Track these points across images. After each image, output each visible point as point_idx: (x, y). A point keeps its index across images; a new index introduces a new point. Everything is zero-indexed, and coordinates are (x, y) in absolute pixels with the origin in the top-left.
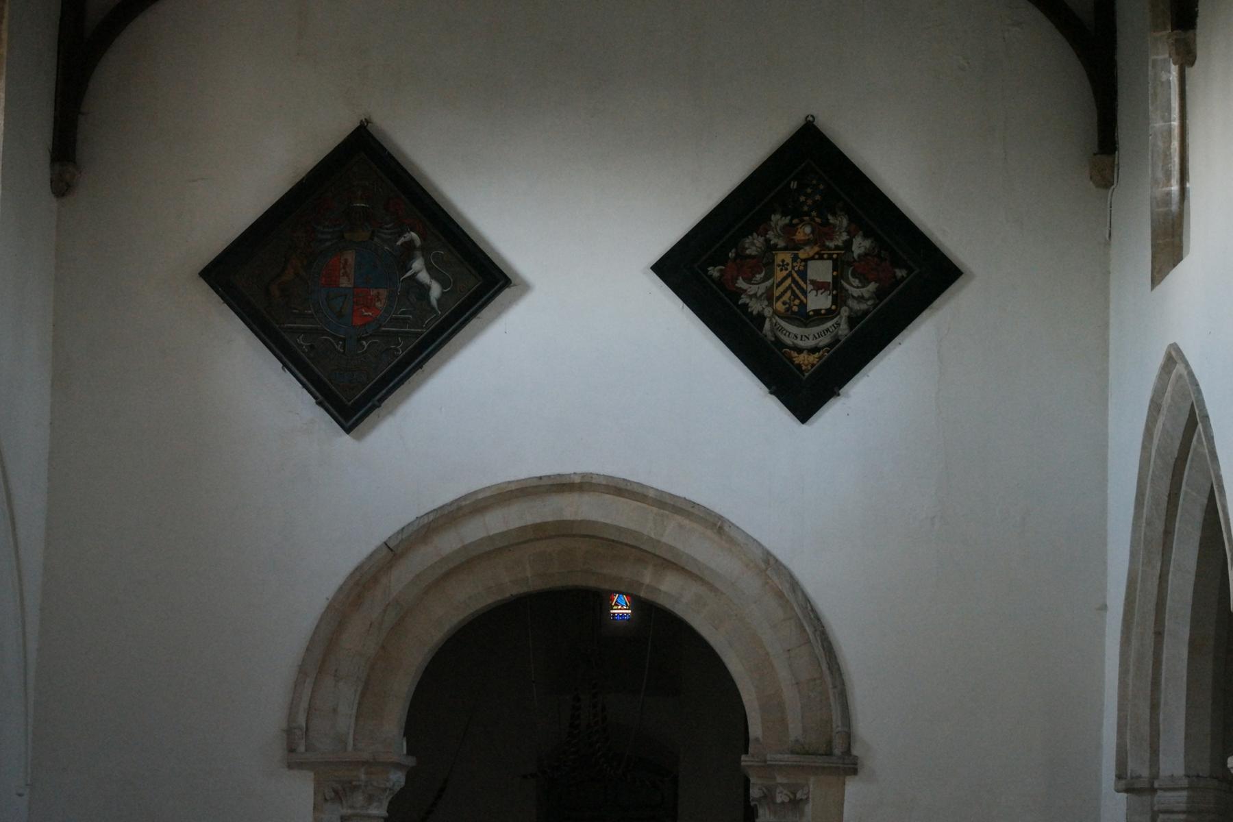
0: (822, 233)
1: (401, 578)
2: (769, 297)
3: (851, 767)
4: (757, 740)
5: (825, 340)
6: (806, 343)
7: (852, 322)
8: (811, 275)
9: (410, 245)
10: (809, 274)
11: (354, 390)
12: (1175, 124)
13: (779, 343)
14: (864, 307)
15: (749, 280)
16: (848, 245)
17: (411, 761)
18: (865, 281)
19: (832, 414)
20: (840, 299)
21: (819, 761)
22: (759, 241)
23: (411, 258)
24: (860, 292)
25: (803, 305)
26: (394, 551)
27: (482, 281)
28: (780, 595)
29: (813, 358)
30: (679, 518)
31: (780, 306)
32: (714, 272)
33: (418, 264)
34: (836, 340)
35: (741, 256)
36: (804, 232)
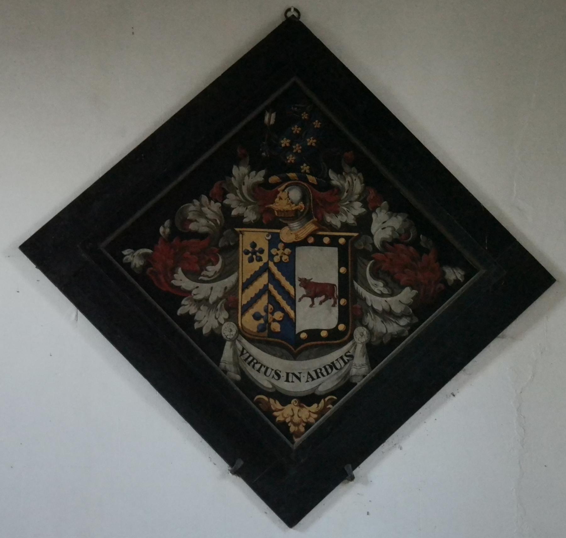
5: (328, 383)
6: (299, 388)
7: (375, 351)
13: (249, 386)
14: (393, 328)
15: (194, 275)
16: (364, 223)
20: (352, 313)
22: (212, 209)
24: (387, 304)
25: (289, 322)
29: (307, 413)
31: (249, 322)
32: (134, 258)
34: (347, 384)
35: (181, 233)
36: (290, 197)
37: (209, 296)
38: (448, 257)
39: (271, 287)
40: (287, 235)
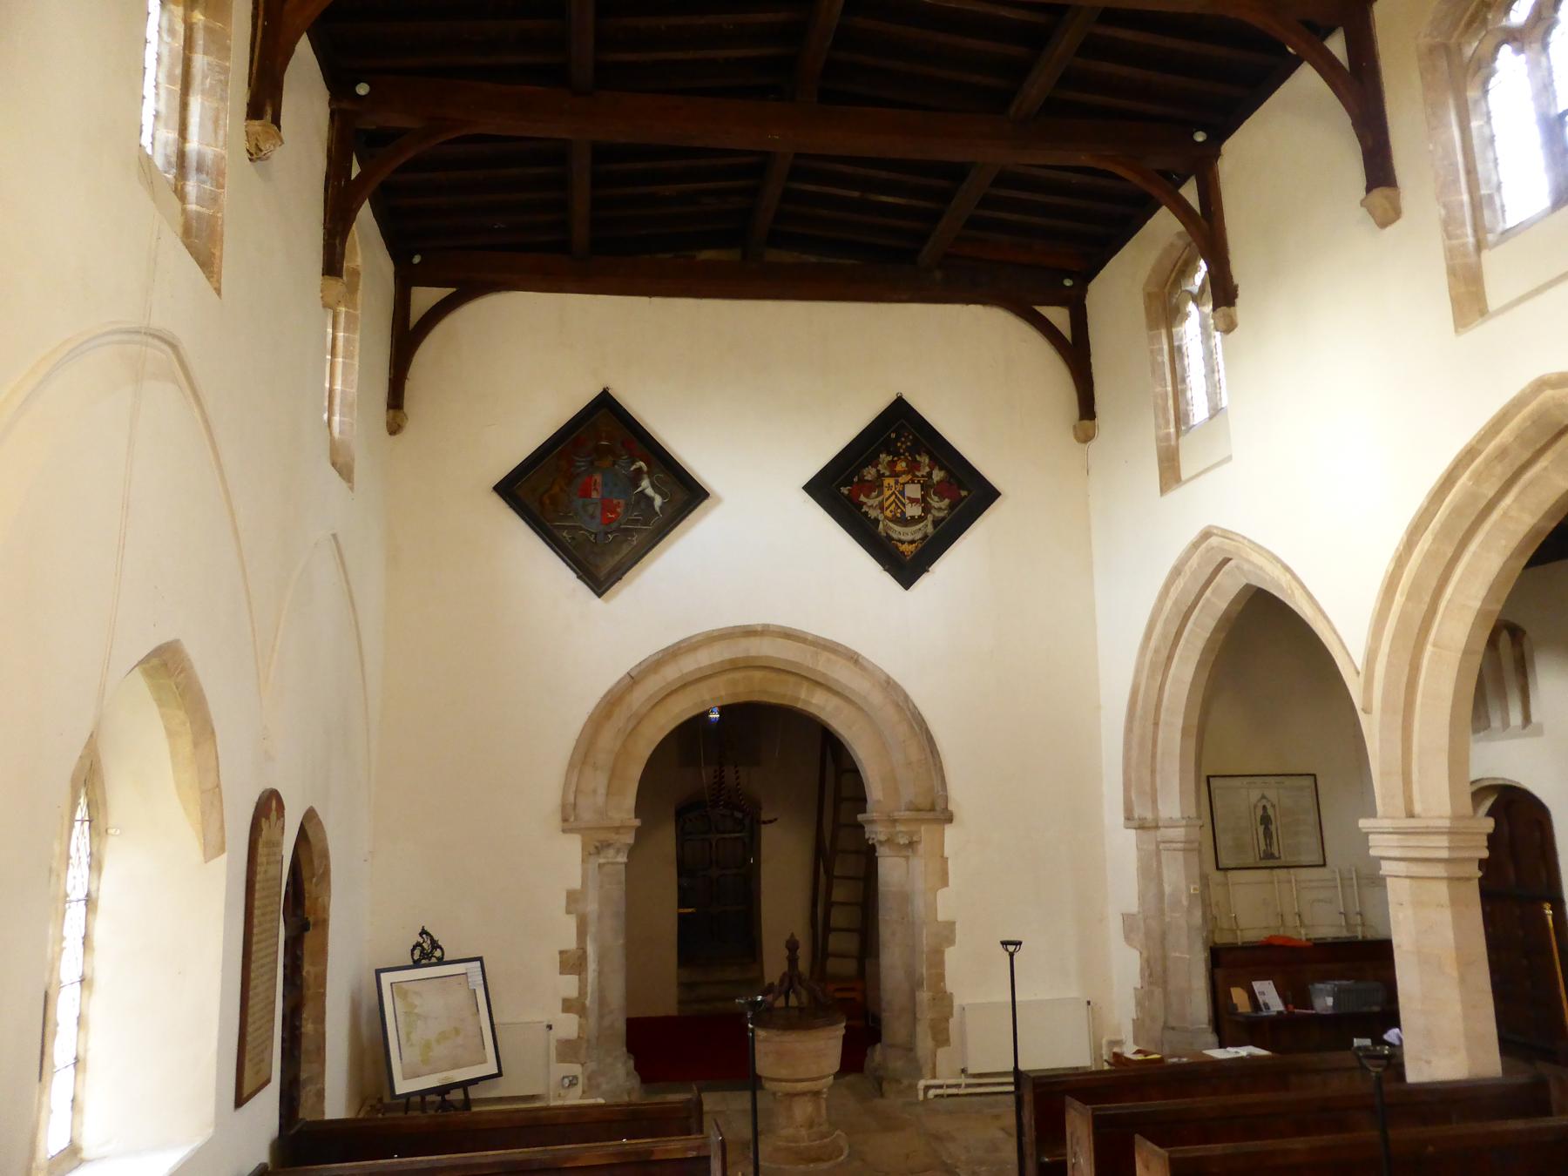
0: (913, 466)
1: (639, 698)
2: (881, 507)
3: (950, 819)
4: (879, 802)
5: (918, 536)
6: (907, 537)
7: (936, 523)
8: (907, 494)
9: (640, 469)
10: (906, 491)
11: (599, 568)
12: (1169, 389)
13: (889, 538)
14: (942, 514)
15: (867, 496)
16: (930, 475)
17: (637, 823)
18: (942, 498)
19: (924, 583)
20: (927, 509)
21: (930, 815)
22: (873, 471)
23: (641, 479)
24: (940, 505)
25: (903, 513)
26: (633, 680)
27: (688, 494)
28: (898, 705)
29: (912, 547)
30: (826, 654)
31: (888, 513)
32: (845, 490)
33: (645, 483)
34: (926, 536)
35: (862, 480)
36: (901, 466)
37: (406, 340)
38: (961, 486)
39: (1112, 1108)
40: (902, 480)
